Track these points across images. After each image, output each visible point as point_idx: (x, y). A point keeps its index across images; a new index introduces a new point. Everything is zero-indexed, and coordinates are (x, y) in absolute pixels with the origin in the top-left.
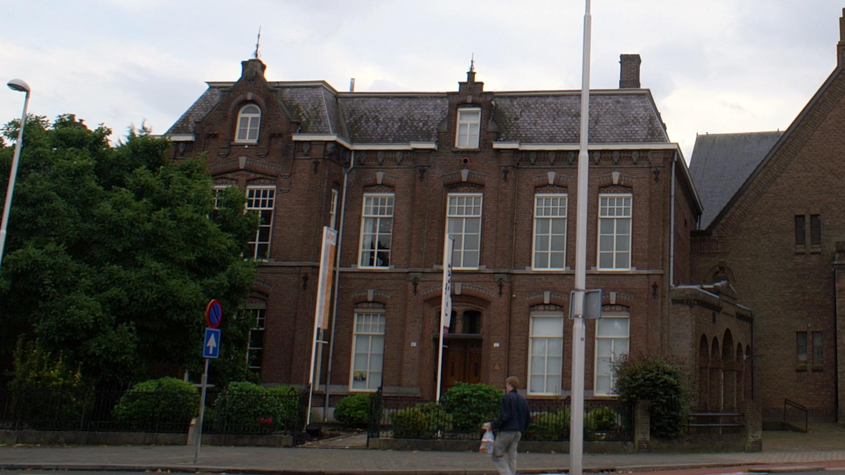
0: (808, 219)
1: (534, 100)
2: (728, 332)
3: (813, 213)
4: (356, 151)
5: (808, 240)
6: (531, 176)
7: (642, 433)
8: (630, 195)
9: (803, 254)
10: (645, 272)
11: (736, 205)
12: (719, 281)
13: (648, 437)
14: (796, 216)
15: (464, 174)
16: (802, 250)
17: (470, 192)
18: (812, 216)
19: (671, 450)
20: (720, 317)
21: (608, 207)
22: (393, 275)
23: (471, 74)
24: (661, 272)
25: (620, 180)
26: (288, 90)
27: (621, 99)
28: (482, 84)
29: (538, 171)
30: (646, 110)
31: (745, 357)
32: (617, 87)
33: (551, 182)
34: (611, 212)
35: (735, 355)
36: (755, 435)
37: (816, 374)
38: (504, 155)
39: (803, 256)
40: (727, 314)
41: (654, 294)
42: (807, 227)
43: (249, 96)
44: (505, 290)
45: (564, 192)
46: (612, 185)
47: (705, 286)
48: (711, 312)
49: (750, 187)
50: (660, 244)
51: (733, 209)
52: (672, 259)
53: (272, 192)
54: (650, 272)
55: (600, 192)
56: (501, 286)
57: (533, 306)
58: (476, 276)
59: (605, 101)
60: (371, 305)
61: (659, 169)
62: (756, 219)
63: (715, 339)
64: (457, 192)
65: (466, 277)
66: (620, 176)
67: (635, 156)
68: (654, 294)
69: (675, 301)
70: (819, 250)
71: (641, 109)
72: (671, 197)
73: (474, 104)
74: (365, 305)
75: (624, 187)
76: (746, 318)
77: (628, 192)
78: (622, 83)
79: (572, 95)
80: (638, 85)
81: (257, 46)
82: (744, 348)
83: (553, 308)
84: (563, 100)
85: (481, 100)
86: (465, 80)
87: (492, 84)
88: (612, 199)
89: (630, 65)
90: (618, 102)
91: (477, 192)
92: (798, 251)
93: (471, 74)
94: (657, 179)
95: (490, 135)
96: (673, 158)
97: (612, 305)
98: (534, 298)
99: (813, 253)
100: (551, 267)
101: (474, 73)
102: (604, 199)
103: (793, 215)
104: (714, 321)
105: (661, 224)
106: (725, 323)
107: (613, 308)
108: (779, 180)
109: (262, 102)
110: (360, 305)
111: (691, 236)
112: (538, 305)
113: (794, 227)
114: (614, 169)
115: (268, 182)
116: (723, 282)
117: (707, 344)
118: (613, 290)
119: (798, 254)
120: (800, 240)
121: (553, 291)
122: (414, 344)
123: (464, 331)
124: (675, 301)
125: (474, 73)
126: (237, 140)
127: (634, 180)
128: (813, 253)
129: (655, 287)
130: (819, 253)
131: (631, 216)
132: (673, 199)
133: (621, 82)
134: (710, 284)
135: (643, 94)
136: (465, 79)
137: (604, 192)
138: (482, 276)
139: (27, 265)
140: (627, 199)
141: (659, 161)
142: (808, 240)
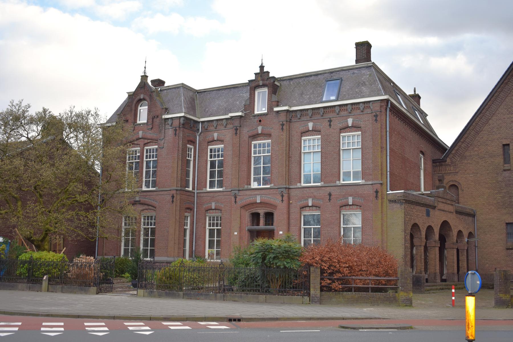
1: (303, 79)
2: (445, 225)
4: (203, 122)
6: (297, 127)
10: (370, 183)
11: (462, 140)
15: (260, 129)
17: (264, 140)
22: (225, 193)
23: (262, 67)
26: (165, 91)
27: (356, 71)
28: (256, 74)
29: (303, 122)
32: (354, 63)
33: (311, 129)
38: (281, 114)
39: (509, 172)
43: (142, 97)
44: (285, 198)
45: (319, 135)
46: (348, 127)
48: (424, 209)
50: (380, 163)
51: (460, 144)
52: (388, 173)
53: (157, 149)
56: (282, 196)
57: (303, 208)
58: (268, 190)
60: (214, 211)
63: (430, 229)
64: (257, 140)
65: (263, 191)
67: (361, 106)
69: (391, 201)
73: (264, 86)
74: (211, 211)
75: (355, 127)
81: (145, 68)
82: (465, 233)
83: (314, 208)
84: (319, 77)
85: (267, 82)
86: (258, 71)
87: (276, 71)
89: (364, 49)
90: (353, 73)
91: (268, 139)
92: (505, 168)
93: (262, 67)
94: (376, 120)
95: (274, 103)
97: (350, 205)
98: (303, 203)
100: (314, 182)
101: (264, 67)
103: (501, 145)
107: (351, 207)
108: (490, 122)
109: (147, 98)
110: (208, 211)
111: (433, 163)
112: (305, 207)
113: (502, 153)
114: (348, 117)
115: (154, 144)
117: (420, 230)
119: (505, 170)
121: (314, 198)
122: (236, 233)
123: (425, 190)
124: (391, 201)
125: (264, 67)
126: (138, 122)
129: (377, 192)
135: (370, 66)
136: (258, 71)
138: (272, 190)
141: (377, 107)
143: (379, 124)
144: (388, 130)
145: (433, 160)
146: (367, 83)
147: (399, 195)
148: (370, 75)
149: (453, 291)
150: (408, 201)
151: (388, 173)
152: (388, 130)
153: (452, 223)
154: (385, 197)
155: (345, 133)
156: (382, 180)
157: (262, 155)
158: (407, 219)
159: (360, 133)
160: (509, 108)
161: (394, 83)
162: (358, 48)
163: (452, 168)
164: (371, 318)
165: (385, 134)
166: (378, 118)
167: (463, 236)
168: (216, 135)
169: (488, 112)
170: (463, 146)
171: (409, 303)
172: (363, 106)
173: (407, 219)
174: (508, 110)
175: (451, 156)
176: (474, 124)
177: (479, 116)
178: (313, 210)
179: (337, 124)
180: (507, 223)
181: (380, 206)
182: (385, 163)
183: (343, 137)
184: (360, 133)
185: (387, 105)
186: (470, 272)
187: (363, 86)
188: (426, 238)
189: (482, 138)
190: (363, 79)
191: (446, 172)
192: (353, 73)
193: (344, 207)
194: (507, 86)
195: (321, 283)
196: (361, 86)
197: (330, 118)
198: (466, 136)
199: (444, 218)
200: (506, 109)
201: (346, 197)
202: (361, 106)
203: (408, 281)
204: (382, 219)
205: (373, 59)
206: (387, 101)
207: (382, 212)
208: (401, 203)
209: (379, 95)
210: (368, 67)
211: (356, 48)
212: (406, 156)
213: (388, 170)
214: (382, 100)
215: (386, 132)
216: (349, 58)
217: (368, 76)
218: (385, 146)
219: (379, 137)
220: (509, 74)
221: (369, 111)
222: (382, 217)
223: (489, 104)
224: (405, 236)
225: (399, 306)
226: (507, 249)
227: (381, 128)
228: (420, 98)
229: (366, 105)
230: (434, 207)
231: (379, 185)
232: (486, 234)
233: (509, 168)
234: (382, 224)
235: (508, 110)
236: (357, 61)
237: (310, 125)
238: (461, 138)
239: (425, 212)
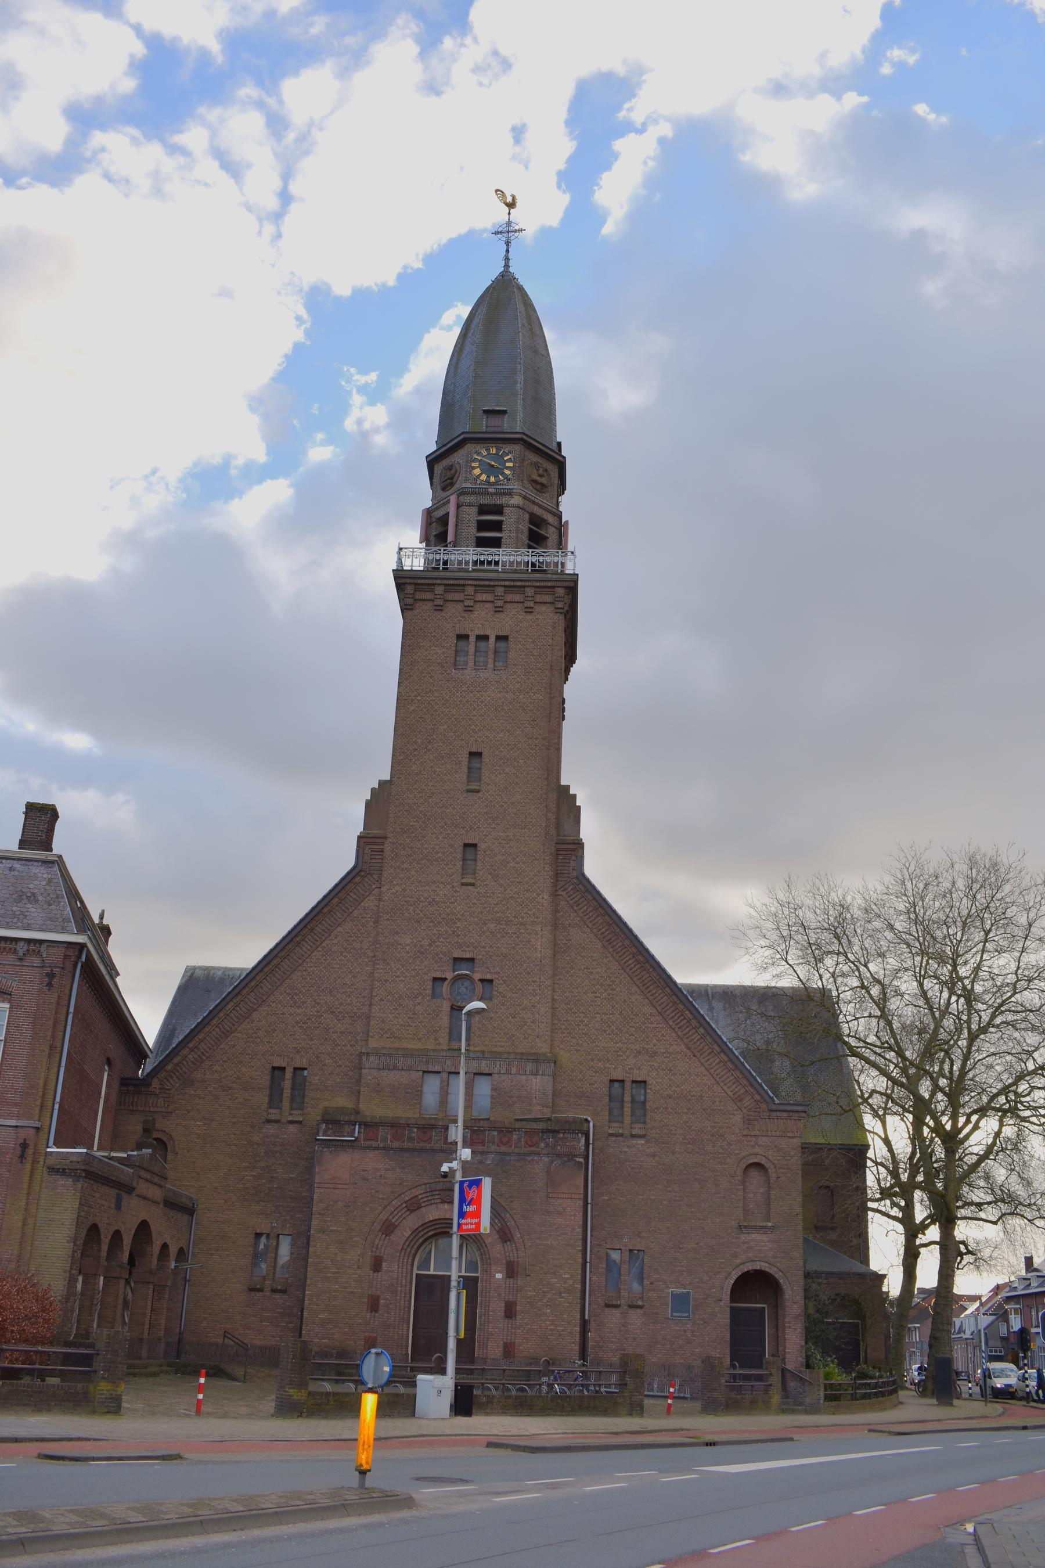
0: (289, 1074)
2: (144, 1227)
3: (298, 1065)
5: (286, 1104)
9: (277, 1121)
10: (13, 1123)
11: (191, 1045)
14: (274, 1068)
24: (37, 1124)
27: (17, 865)
31: (173, 1265)
32: (15, 847)
35: (155, 1260)
37: (277, 1296)
39: (276, 1125)
40: (145, 1198)
41: (22, 1157)
42: (287, 1084)
48: (113, 1192)
50: (41, 1082)
51: (186, 1051)
62: (217, 1067)
63: (117, 1235)
67: (22, 948)
68: (22, 1157)
69: (53, 1170)
76: (182, 1208)
80: (51, 850)
82: (173, 1250)
92: (270, 1117)
94: (50, 985)
99: (291, 1122)
103: (269, 1067)
105: (47, 1050)
106: (135, 1212)
108: (255, 1015)
113: (268, 1083)
117: (99, 1240)
119: (268, 1121)
124: (53, 1170)
127: (14, 984)
128: (291, 1122)
129: (24, 1146)
130: (300, 1122)
133: (21, 841)
135: (52, 862)
139: (832, 1361)
141: (56, 956)
142: (286, 1104)
143: (56, 995)
144: (72, 1009)
145: (122, 1079)
146: (40, 898)
147: (75, 1159)
148: (50, 881)
149: (202, 1380)
150: (91, 1174)
151: (57, 1106)
152: (72, 1009)
153: (155, 1227)
154: (42, 1159)
156: (39, 1120)
158: (83, 1214)
159: (8, 1006)
160: (296, 994)
161: (82, 902)
162: (31, 814)
163: (160, 1102)
164: (71, 1439)
165: (63, 1017)
166: (55, 981)
167: (169, 1256)
169: (252, 994)
170: (190, 1057)
171: (113, 1407)
172: (25, 948)
173: (83, 1214)
174: (292, 998)
175: (163, 1074)
176: (221, 1014)
177: (235, 1001)
181: (26, 1179)
182: (54, 1083)
184: (8, 1006)
185: (79, 956)
186: (373, 1351)
188: (108, 1259)
189: (234, 1046)
190: (31, 886)
191: (147, 1109)
192: (11, 869)
194: (298, 949)
195: (966, 1399)
196: (25, 901)
198: (201, 1036)
199: (143, 1216)
200: (288, 994)
202: (22, 948)
203: (119, 1359)
204: (26, 1210)
205: (59, 845)
206: (82, 946)
207: (28, 1194)
208: (77, 1178)
209: (64, 930)
210: (45, 862)
211: (26, 813)
212: (85, 1067)
213: (58, 1099)
214: (70, 944)
215: (68, 1014)
217: (44, 883)
218: (59, 1045)
219: (51, 1023)
220: (305, 926)
221: (36, 961)
222: (27, 1204)
223: (258, 978)
224: (74, 1252)
225: (93, 1412)
226: (251, 1290)
227: (58, 1004)
228: (109, 933)
229: (32, 947)
230: (130, 1190)
231: (32, 1132)
232: (212, 1254)
233: (278, 1117)
234: (25, 1221)
235: (292, 998)
236: (23, 844)
238: (191, 1041)
239: (114, 1201)
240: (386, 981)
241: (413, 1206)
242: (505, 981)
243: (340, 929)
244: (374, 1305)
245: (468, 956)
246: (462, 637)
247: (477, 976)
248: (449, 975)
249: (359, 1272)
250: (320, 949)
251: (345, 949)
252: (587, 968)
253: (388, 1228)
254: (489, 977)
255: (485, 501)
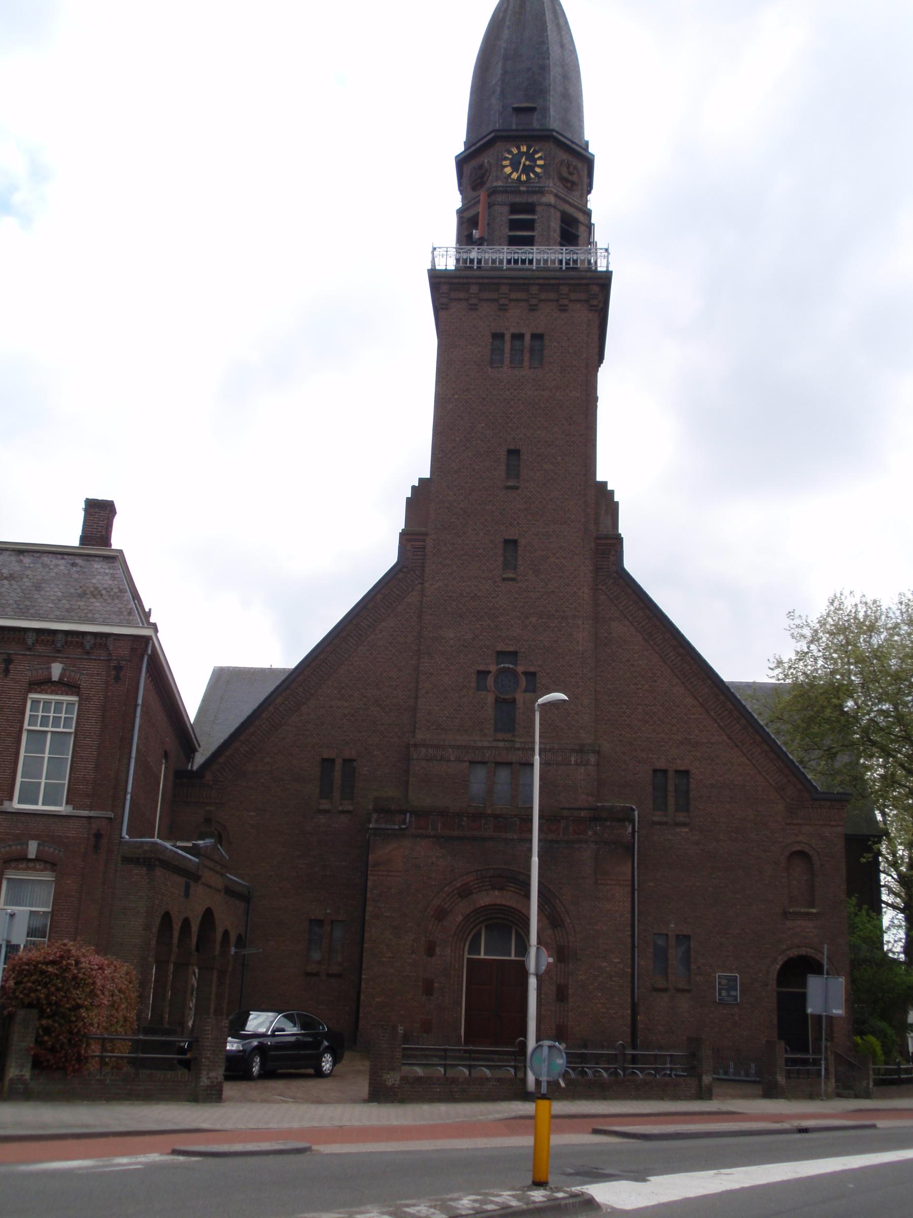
2: (208, 914)
7: (228, 1073)
8: (75, 699)
10: (85, 813)
12: (203, 839)
13: (27, 1073)
16: (326, 807)
18: (345, 761)
19: (69, 1096)
20: (198, 890)
21: (40, 714)
25: (62, 675)
27: (79, 561)
30: (113, 577)
31: (233, 950)
32: (76, 543)
34: (45, 721)
36: (212, 1074)
40: (209, 886)
42: (337, 774)
47: (179, 844)
48: (181, 880)
49: (264, 715)
52: (129, 797)
54: (92, 814)
55: (30, 691)
59: (55, 561)
61: (123, 663)
63: (186, 923)
66: (64, 670)
69: (127, 860)
70: (351, 808)
71: (106, 578)
72: (136, 705)
75: (66, 686)
77: (72, 694)
78: (84, 539)
79: (6, 550)
80: (110, 545)
82: (233, 938)
88: (47, 703)
89: (100, 515)
90: (74, 565)
92: (322, 807)
94: (117, 678)
96: (146, 650)
102: (36, 702)
104: (187, 894)
107: (31, 865)
116: (209, 841)
118: (34, 838)
119: (320, 812)
120: (326, 791)
124: (127, 860)
127: (83, 678)
129: (98, 836)
131: (73, 730)
132: (139, 708)
134: (188, 840)
137: (36, 692)
140: (70, 704)
142: (671, 808)
155: (40, 692)
157: (50, 729)
168: (56, 670)
172: (93, 641)
178: (35, 870)
179: (24, 670)
180: (311, 920)
183: (33, 702)
187: (94, 596)
190: (94, 581)
193: (13, 864)
197: (9, 654)
201: (22, 839)
205: (117, 542)
216: (68, 532)
229: (99, 641)
237: (56, 670)
240: (432, 674)
241: (465, 893)
242: (548, 674)
243: (384, 624)
244: (428, 989)
245: (511, 649)
246: (498, 336)
247: (520, 669)
248: (493, 668)
249: (413, 956)
250: (365, 644)
251: (391, 643)
252: (628, 661)
253: (441, 914)
254: (532, 669)
255: (518, 199)
